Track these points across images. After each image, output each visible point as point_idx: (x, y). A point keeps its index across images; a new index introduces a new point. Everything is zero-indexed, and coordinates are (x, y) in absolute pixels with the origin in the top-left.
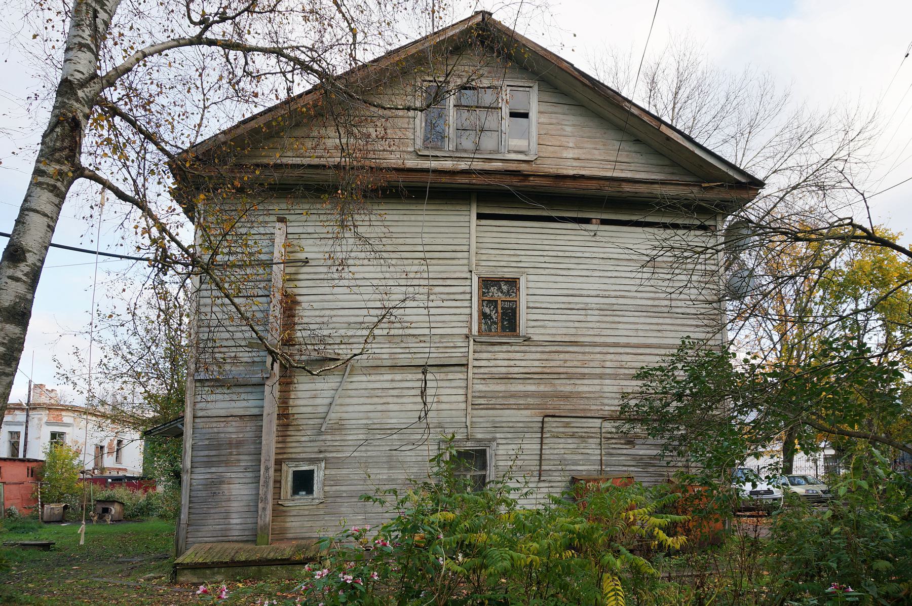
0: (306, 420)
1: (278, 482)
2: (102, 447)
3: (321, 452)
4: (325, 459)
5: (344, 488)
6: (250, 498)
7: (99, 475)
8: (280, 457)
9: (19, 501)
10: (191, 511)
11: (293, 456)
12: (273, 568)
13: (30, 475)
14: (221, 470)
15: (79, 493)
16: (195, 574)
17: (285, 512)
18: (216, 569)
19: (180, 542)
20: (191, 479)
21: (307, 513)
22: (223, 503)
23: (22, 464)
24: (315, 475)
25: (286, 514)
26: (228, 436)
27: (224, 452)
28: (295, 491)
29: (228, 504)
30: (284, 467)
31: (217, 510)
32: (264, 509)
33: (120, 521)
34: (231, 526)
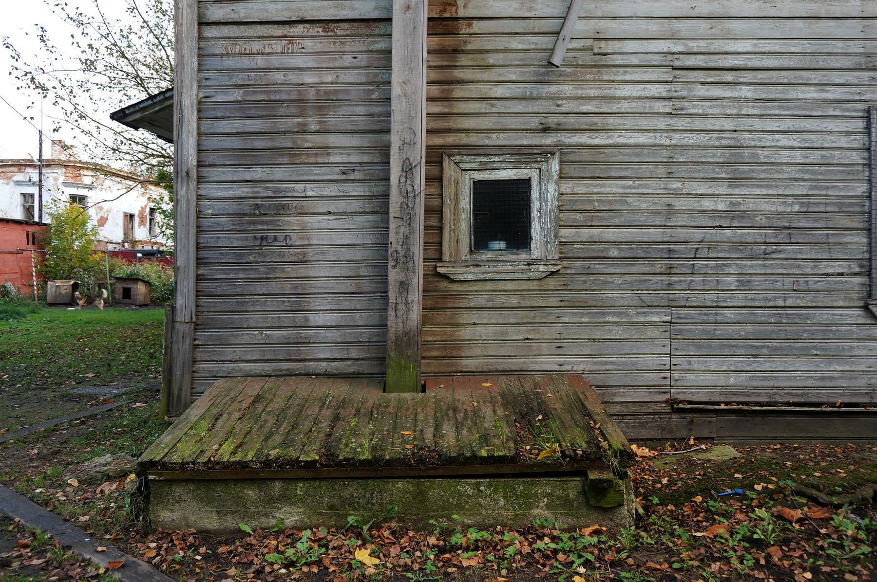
0: (506, 39)
1: (435, 212)
2: (132, 216)
3: (546, 130)
4: (560, 149)
5: (611, 234)
6: (359, 255)
7: (130, 249)
8: (438, 141)
9: (18, 276)
10: (205, 286)
11: (473, 139)
12: (466, 487)
13: (30, 242)
14: (278, 173)
15: (96, 268)
16: (209, 502)
17: (455, 296)
18: (278, 485)
19: (177, 372)
20: (199, 197)
21: (513, 301)
22: (288, 268)
23: (19, 227)
24: (535, 194)
25: (458, 303)
26: (293, 78)
27: (283, 124)
28: (480, 242)
29: (302, 270)
30: (450, 170)
31: (274, 287)
32: (404, 286)
33: (146, 305)
34: (312, 332)
